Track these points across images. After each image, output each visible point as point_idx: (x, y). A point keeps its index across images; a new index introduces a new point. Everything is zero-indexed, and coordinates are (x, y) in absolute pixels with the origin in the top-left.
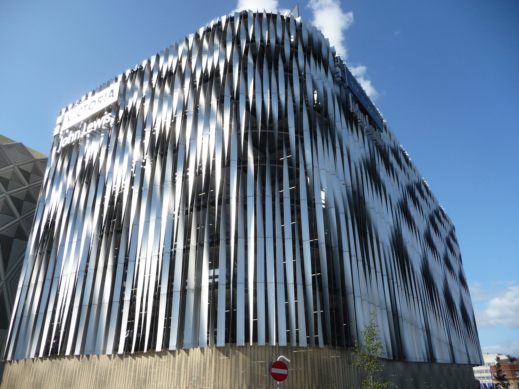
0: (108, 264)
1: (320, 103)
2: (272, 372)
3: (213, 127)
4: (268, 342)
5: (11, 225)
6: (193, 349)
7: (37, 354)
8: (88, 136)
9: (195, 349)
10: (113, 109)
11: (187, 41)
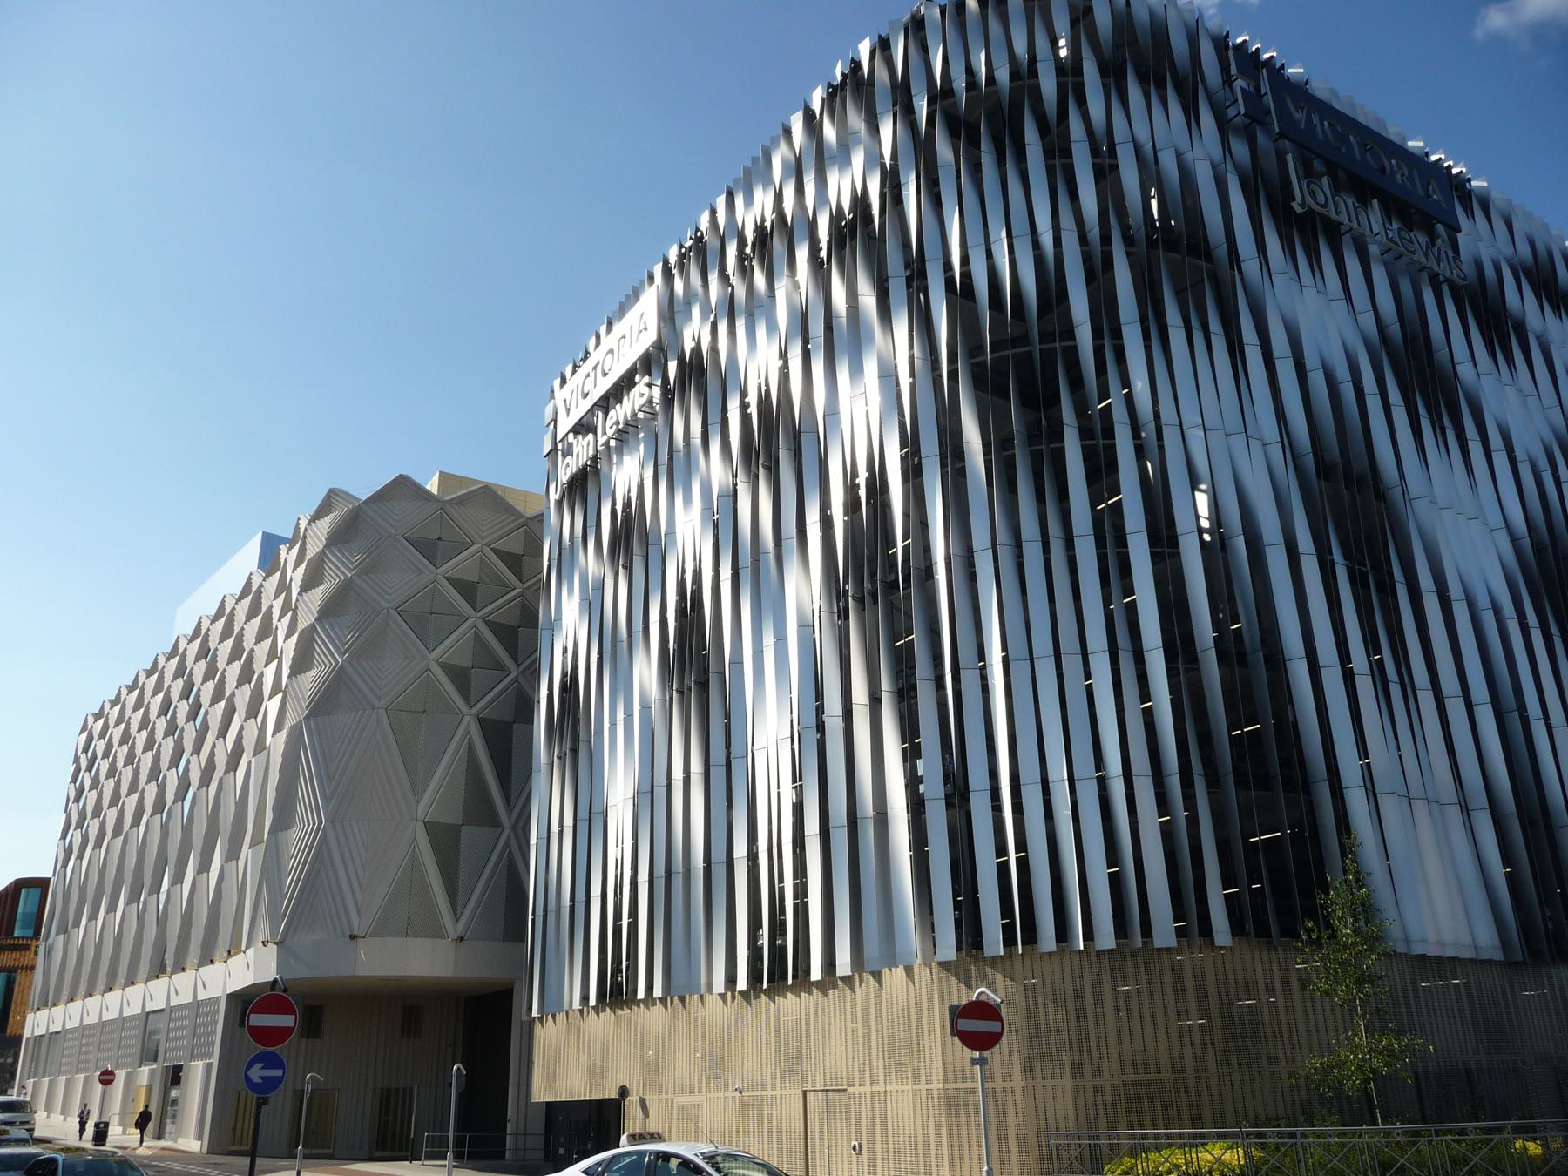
0: (692, 771)
1: (1173, 223)
2: (959, 1028)
3: (871, 367)
4: (1126, 937)
5: (499, 694)
6: (891, 970)
7: (585, 998)
8: (613, 443)
9: (893, 969)
10: (649, 363)
11: (787, 132)
